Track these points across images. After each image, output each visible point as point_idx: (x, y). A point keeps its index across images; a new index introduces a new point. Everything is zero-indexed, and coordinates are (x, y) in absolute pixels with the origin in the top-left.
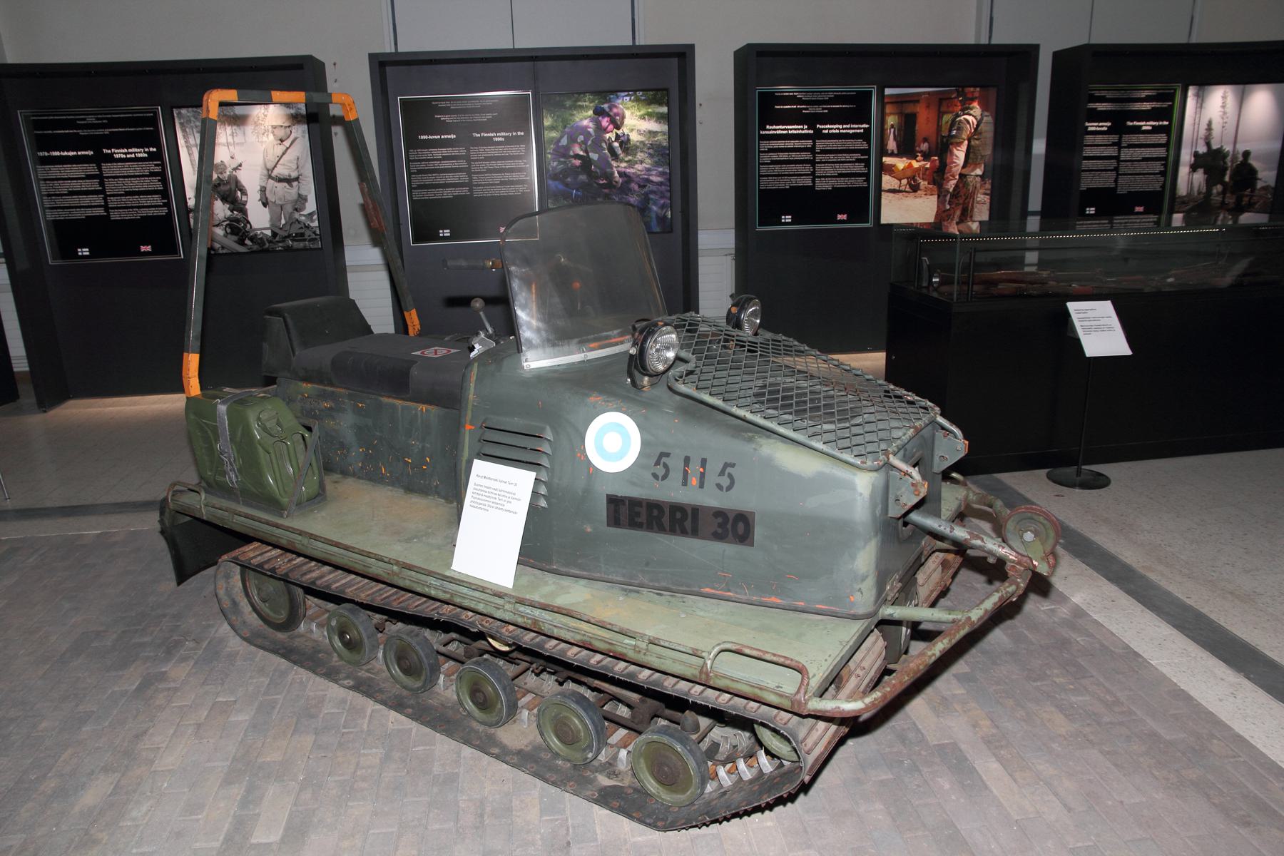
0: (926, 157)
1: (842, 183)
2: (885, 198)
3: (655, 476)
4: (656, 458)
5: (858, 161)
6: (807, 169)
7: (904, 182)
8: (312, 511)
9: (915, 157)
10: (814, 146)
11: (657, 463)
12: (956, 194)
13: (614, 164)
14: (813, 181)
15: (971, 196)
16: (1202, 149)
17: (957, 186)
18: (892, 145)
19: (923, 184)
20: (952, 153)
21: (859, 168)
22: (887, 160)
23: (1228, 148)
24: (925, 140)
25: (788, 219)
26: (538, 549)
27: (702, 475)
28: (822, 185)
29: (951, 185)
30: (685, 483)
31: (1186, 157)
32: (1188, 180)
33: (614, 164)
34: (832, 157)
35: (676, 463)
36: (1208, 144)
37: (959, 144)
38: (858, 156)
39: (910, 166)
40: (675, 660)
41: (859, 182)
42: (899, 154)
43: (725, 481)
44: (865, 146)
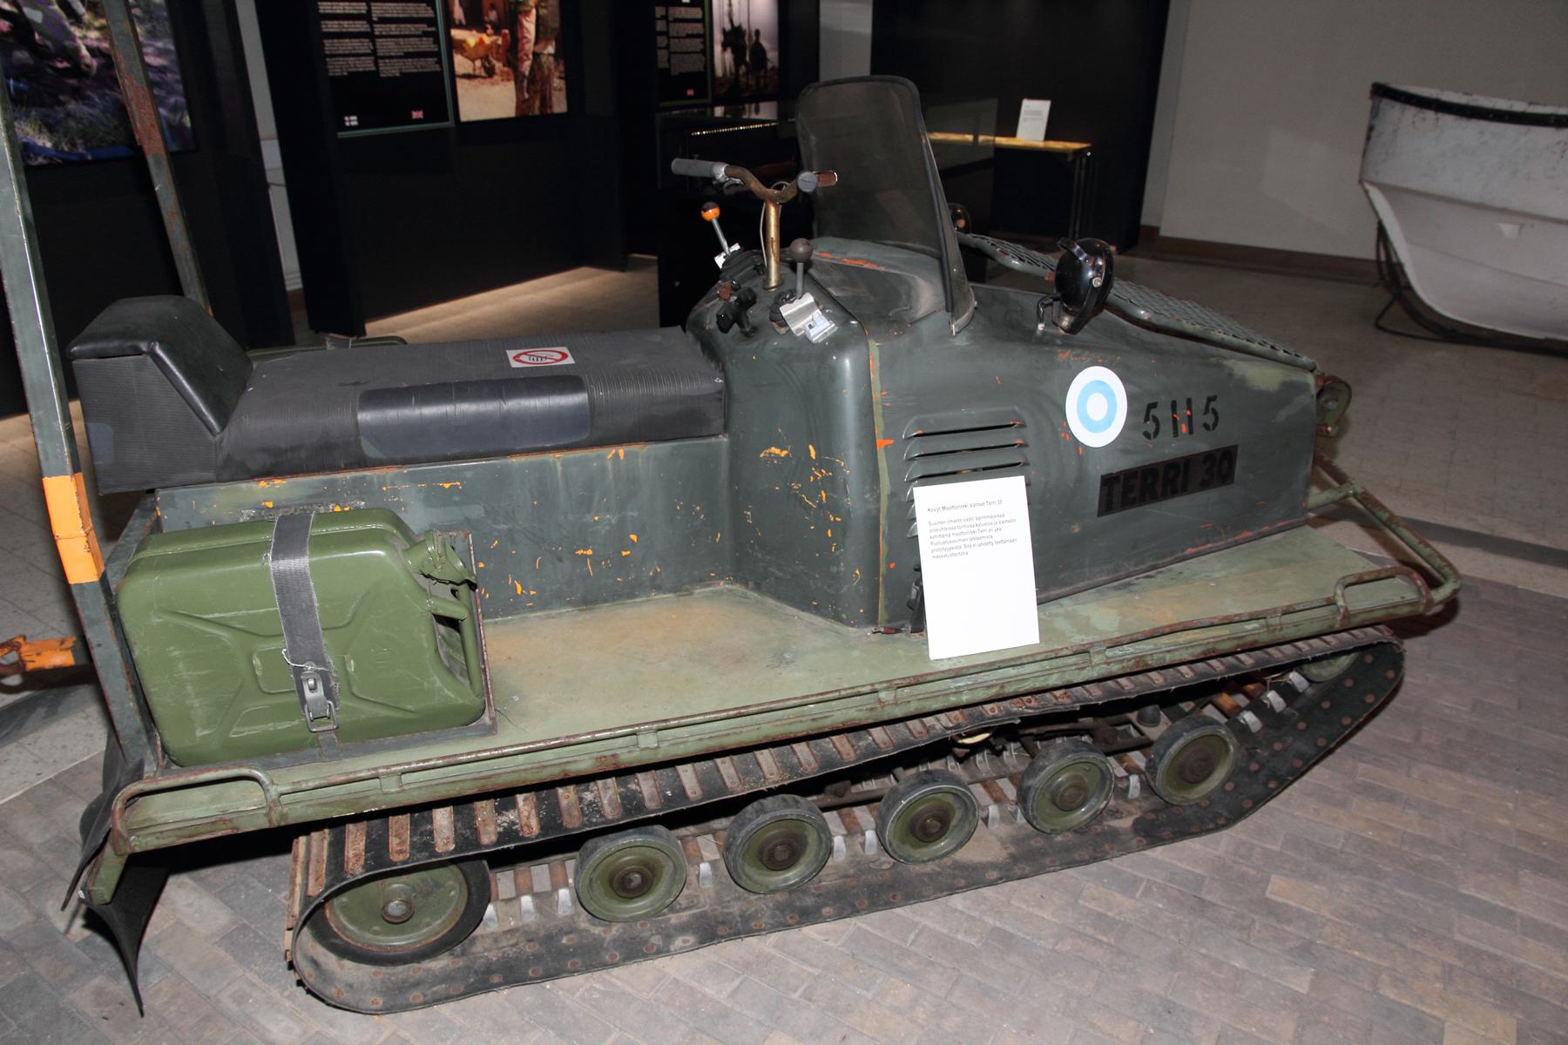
0: (497, 32)
1: (411, 66)
2: (462, 86)
3: (1147, 435)
4: (1144, 413)
5: (426, 34)
6: (364, 46)
7: (478, 63)
8: (29, 724)
9: (484, 30)
10: (369, 11)
11: (1147, 419)
12: (532, 79)
13: (77, 32)
14: (376, 64)
15: (547, 80)
16: (728, 27)
17: (532, 68)
18: (458, 13)
19: (498, 66)
20: (522, 26)
21: (427, 45)
22: (457, 34)
23: (745, 27)
24: (493, 7)
25: (418, 115)
26: (1058, 568)
27: (1190, 418)
28: (390, 70)
29: (526, 66)
30: (1176, 433)
31: (718, 37)
32: (722, 59)
33: (77, 32)
34: (393, 28)
35: (1163, 413)
36: (731, 21)
37: (527, 13)
38: (424, 27)
39: (481, 42)
40: (1312, 620)
41: (429, 65)
42: (467, 26)
43: (1210, 419)
44: (429, 14)
